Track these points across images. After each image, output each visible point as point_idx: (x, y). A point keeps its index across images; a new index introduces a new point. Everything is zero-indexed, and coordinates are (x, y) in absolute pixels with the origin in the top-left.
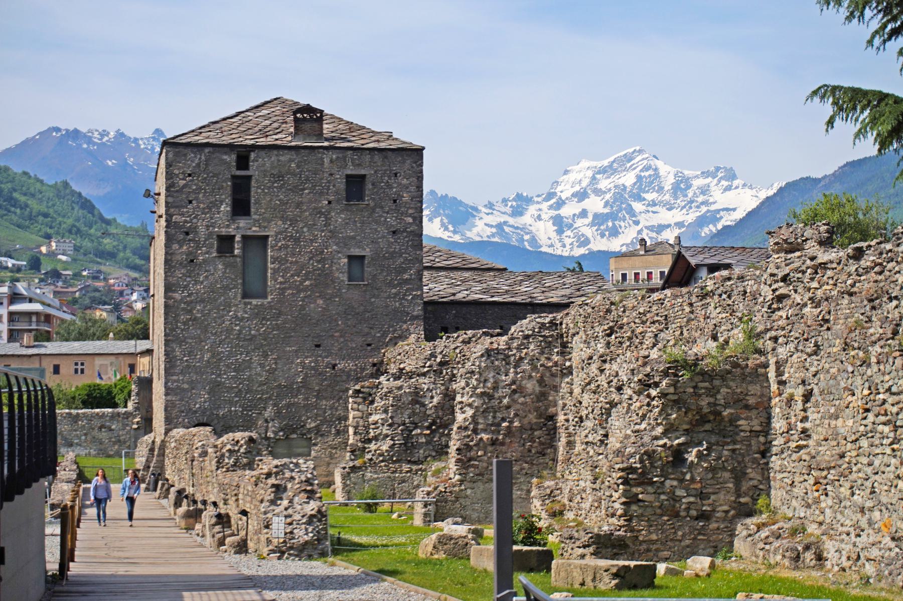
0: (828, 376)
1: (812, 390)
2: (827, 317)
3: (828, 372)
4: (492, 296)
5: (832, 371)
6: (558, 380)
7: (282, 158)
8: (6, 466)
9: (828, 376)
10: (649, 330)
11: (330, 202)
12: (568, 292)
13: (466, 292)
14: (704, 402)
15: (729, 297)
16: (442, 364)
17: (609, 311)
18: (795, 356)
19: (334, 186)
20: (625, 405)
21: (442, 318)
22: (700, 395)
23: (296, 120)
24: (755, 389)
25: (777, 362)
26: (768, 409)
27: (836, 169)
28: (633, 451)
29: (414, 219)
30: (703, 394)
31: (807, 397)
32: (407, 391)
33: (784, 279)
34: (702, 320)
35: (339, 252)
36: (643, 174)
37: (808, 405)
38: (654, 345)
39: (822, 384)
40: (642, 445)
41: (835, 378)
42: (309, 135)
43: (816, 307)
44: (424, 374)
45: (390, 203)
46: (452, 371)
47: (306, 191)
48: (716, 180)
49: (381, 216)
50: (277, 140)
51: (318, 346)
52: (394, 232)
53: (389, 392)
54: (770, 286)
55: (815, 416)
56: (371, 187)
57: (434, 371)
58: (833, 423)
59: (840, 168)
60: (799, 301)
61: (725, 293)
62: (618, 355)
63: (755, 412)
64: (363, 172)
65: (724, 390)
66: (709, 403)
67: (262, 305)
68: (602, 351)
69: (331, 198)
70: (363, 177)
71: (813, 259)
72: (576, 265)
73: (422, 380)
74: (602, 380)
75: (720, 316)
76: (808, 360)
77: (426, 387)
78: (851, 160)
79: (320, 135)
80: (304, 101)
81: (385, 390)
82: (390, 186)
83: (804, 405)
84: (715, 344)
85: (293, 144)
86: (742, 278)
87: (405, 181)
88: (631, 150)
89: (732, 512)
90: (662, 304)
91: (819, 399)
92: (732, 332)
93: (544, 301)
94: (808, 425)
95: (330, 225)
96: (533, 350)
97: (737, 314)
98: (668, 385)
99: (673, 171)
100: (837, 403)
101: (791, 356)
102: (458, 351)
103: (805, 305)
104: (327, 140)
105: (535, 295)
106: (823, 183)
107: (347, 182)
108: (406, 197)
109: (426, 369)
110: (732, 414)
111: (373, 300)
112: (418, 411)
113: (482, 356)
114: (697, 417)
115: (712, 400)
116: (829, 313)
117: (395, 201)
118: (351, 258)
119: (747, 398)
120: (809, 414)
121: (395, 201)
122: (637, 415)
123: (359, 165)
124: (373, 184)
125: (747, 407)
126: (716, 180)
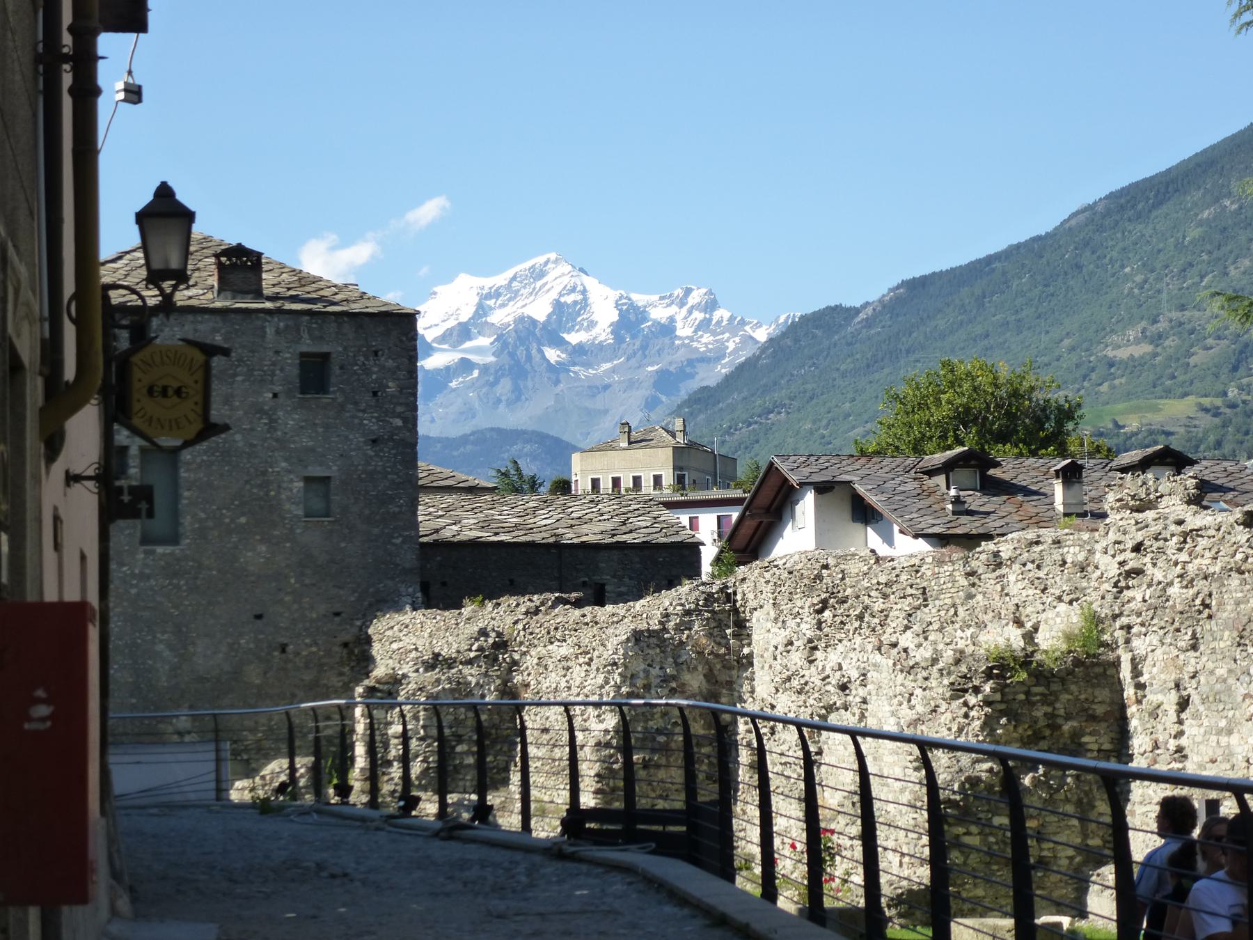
0: (1213, 679)
1: (1189, 696)
2: (1208, 602)
3: (1212, 672)
4: (496, 534)
5: (1219, 672)
6: (734, 672)
7: (199, 327)
8: (671, 828)
9: (1213, 679)
10: (895, 607)
11: (275, 395)
12: (609, 526)
13: (453, 527)
14: (1039, 712)
15: (1039, 567)
16: (496, 646)
17: (819, 577)
18: (1159, 652)
19: (282, 370)
20: (857, 712)
21: (453, 574)
22: (1034, 704)
23: (220, 266)
24: (1103, 694)
25: (1133, 660)
26: (1123, 721)
27: (885, 292)
28: (949, 778)
29: (405, 420)
30: (1038, 701)
31: (1183, 704)
32: (447, 686)
33: (1137, 548)
34: (997, 598)
35: (290, 472)
36: (562, 300)
37: (1183, 716)
38: (907, 628)
39: (1203, 689)
40: (961, 770)
41: (1225, 681)
42: (239, 292)
43: (1186, 587)
44: (470, 662)
45: (368, 397)
46: (511, 656)
47: (239, 378)
48: (685, 310)
49: (353, 417)
50: (190, 298)
51: (259, 617)
52: (374, 441)
53: (420, 689)
54: (1114, 556)
55: (1195, 731)
56: (338, 372)
57: (485, 657)
58: (1224, 740)
59: (891, 290)
60: (1161, 579)
61: (1033, 562)
62: (840, 641)
63: (1104, 725)
64: (325, 348)
65: (1065, 697)
66: (1045, 714)
67: (171, 554)
68: (809, 634)
69: (277, 389)
70: (326, 356)
71: (1180, 522)
72: (510, 465)
73: (467, 670)
74: (812, 675)
75: (1024, 593)
76: (1182, 657)
77: (474, 681)
78: (909, 277)
79: (258, 294)
80: (232, 240)
81: (412, 686)
82: (367, 372)
83: (1178, 716)
84: (1019, 632)
85: (218, 304)
86: (1059, 542)
87: (390, 363)
88: (541, 259)
89: (1078, 859)
90: (917, 572)
91: (1201, 708)
92: (1044, 616)
93: (576, 541)
94: (1184, 741)
95: (276, 430)
96: (697, 632)
97: (1052, 591)
98: (993, 690)
99: (613, 295)
100: (1230, 714)
101: (1153, 651)
102: (520, 626)
103: (1171, 584)
104: (269, 299)
105: (560, 531)
106: (862, 316)
107: (302, 365)
108: (392, 387)
109: (472, 655)
110: (1074, 728)
111: (343, 545)
112: (463, 717)
113: (628, 640)
114: (1030, 733)
115: (1049, 710)
116: (1210, 595)
117: (375, 394)
118: (308, 480)
119: (1094, 707)
120: (1184, 728)
121: (375, 394)
122: (950, 729)
123: (321, 338)
124: (342, 368)
125: (1093, 718)
126: (685, 310)
